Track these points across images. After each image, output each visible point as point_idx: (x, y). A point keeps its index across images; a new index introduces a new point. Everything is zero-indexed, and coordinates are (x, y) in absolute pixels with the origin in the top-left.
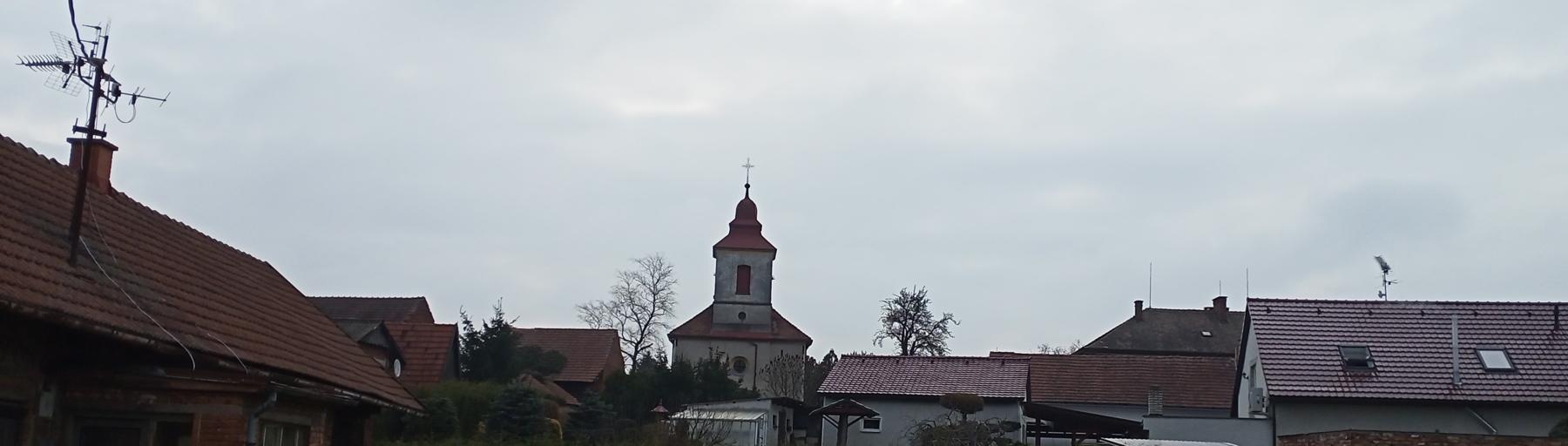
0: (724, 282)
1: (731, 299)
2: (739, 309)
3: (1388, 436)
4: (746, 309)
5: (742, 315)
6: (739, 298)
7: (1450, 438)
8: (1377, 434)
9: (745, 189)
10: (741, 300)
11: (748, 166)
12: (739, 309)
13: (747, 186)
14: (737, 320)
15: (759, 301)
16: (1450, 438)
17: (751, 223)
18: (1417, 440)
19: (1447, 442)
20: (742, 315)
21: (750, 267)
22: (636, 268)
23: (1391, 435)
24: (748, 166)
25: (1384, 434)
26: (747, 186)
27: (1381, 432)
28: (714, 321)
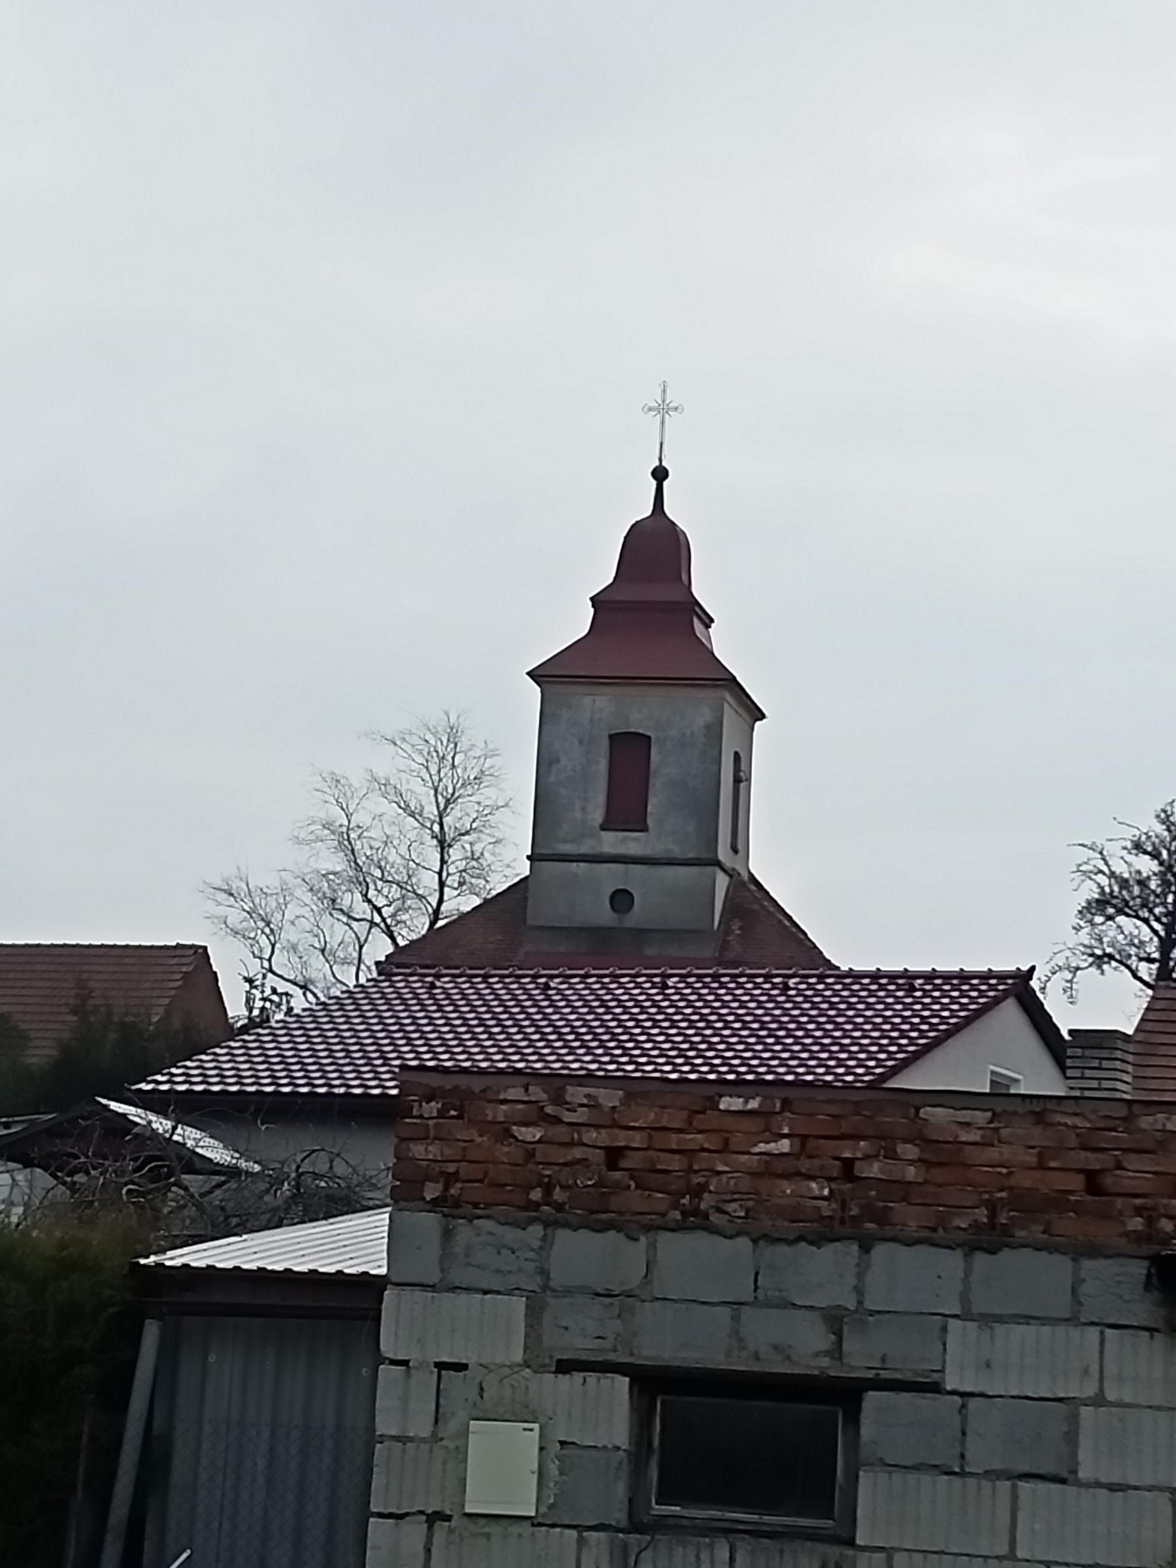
0: (563, 791)
1: (585, 849)
2: (611, 877)
3: (593, 1105)
4: (635, 879)
5: (621, 899)
6: (611, 843)
7: (935, 1114)
8: (537, 1093)
9: (654, 483)
10: (621, 850)
11: (663, 409)
12: (611, 877)
13: (660, 474)
14: (604, 915)
15: (677, 852)
16: (935, 1114)
17: (675, 596)
18: (747, 1124)
19: (919, 1138)
20: (621, 899)
21: (649, 738)
22: (387, 763)
23: (609, 1098)
24: (663, 409)
25: (576, 1094)
26: (660, 474)
27: (556, 1083)
28: (530, 922)
